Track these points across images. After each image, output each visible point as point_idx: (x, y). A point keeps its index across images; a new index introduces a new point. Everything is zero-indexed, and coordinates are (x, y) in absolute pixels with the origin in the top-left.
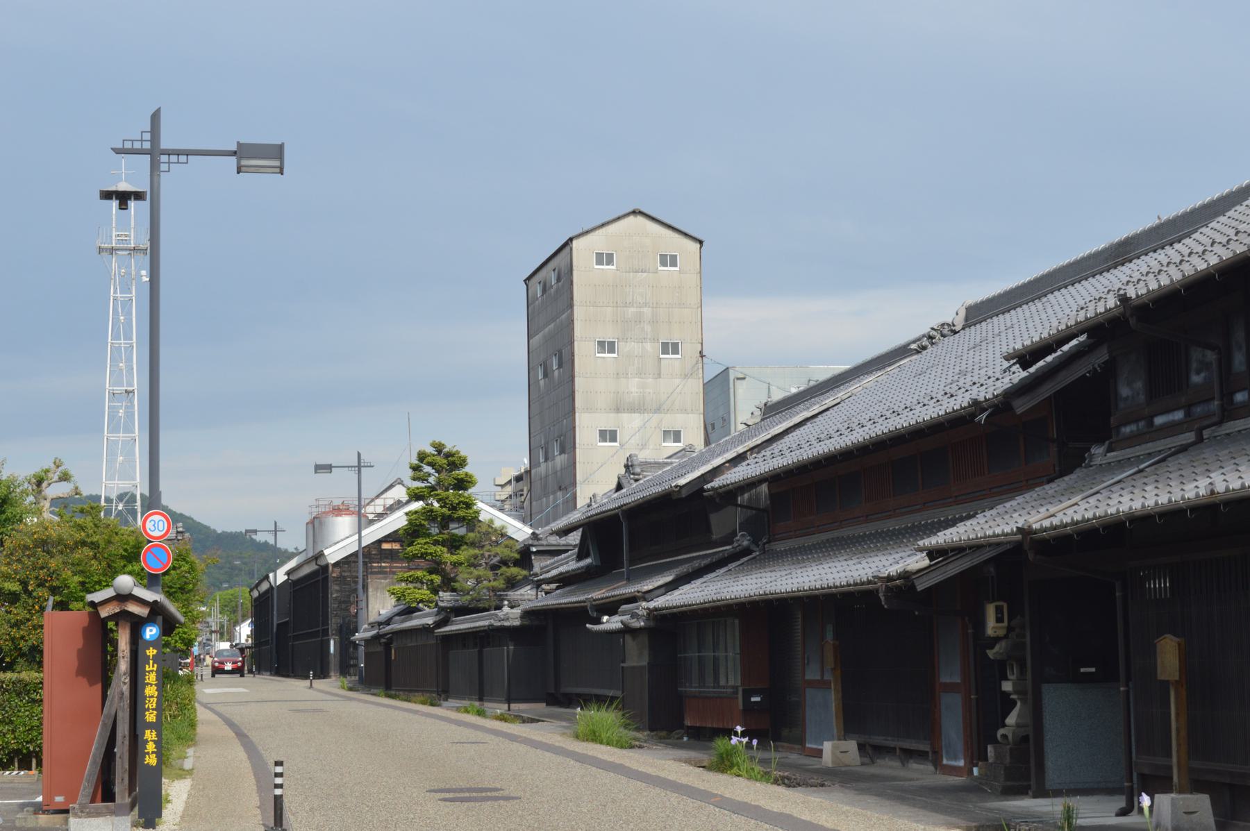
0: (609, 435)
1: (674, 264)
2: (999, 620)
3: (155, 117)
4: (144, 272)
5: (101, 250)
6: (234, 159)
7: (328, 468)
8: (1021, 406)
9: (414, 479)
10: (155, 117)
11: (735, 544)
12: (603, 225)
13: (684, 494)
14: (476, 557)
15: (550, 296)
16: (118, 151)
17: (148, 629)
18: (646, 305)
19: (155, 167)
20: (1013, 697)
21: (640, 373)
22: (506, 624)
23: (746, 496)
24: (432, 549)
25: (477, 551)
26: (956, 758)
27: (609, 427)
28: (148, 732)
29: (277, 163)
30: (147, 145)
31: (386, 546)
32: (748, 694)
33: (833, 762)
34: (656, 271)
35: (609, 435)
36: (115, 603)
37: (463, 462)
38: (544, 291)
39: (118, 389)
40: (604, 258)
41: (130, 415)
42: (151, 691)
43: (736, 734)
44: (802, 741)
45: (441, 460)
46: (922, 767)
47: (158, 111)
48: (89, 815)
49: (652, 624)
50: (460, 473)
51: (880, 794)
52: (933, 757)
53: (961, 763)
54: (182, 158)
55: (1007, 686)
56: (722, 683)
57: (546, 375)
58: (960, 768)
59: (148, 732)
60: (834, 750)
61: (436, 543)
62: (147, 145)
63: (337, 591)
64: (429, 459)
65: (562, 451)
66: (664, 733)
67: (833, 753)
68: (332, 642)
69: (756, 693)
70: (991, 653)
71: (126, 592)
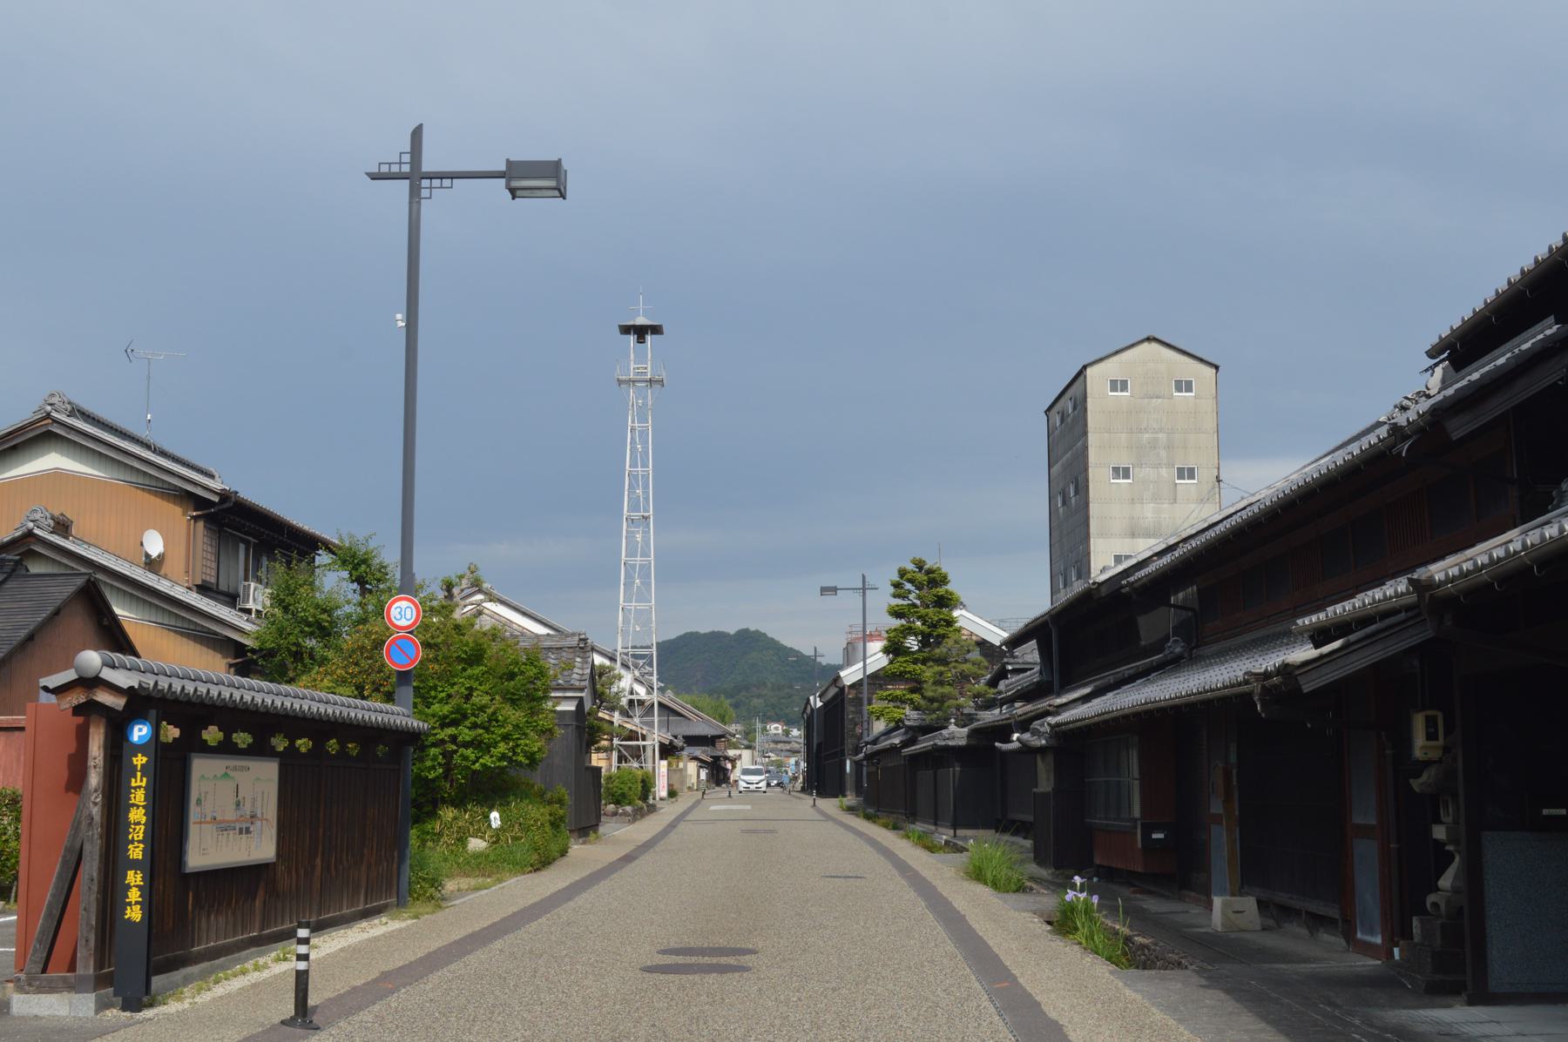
1: (1189, 389)
2: (1431, 736)
3: (417, 134)
4: (399, 316)
5: (620, 382)
6: (503, 181)
7: (834, 590)
8: (1458, 428)
9: (895, 596)
10: (417, 134)
12: (1117, 352)
13: (1104, 591)
14: (941, 674)
15: (1068, 421)
16: (374, 177)
17: (136, 728)
18: (1161, 430)
19: (415, 193)
20: (1450, 848)
21: (1156, 498)
22: (950, 743)
23: (1181, 595)
24: (911, 667)
26: (1372, 933)
28: (131, 873)
29: (552, 183)
30: (406, 168)
36: (78, 690)
37: (944, 580)
38: (1062, 420)
40: (1119, 385)
42: (137, 815)
43: (1073, 887)
45: (921, 577)
47: (420, 127)
48: (39, 990)
50: (941, 591)
51: (1236, 991)
52: (1346, 927)
53: (1378, 940)
54: (447, 182)
55: (1439, 833)
57: (1064, 503)
58: (1376, 945)
59: (131, 873)
60: (1225, 910)
61: (915, 662)
62: (406, 168)
64: (909, 576)
65: (1079, 577)
67: (1223, 913)
70: (1416, 784)
71: (91, 674)
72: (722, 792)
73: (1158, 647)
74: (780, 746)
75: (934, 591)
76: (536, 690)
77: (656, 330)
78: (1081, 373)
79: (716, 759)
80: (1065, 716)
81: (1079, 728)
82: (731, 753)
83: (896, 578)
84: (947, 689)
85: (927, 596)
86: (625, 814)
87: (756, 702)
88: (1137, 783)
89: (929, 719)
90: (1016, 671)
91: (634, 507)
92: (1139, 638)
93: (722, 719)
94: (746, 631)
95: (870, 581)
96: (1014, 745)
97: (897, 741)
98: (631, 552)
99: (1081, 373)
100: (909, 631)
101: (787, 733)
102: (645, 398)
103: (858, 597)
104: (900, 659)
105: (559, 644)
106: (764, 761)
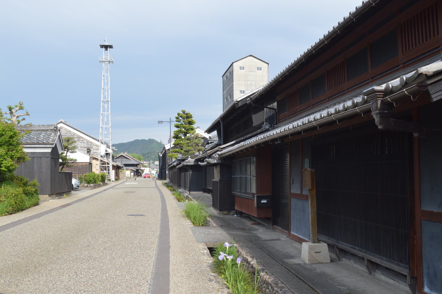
7: (162, 122)
11: (263, 128)
12: (242, 59)
13: (240, 105)
14: (188, 143)
18: (253, 81)
22: (189, 164)
25: (188, 141)
32: (259, 198)
33: (309, 260)
34: (256, 72)
37: (191, 117)
39: (105, 100)
40: (242, 68)
41: (108, 108)
45: (184, 116)
46: (391, 281)
49: (220, 161)
50: (190, 120)
56: (248, 191)
57: (227, 101)
64: (180, 115)
66: (226, 212)
67: (310, 253)
69: (264, 198)
72: (138, 179)
73: (260, 126)
75: (188, 120)
76: (13, 141)
77: (111, 47)
78: (232, 65)
79: (137, 170)
80: (224, 151)
81: (230, 155)
82: (142, 168)
83: (177, 116)
84: (190, 148)
85: (186, 122)
86: (90, 187)
87: (153, 156)
88: (254, 178)
89: (184, 157)
90: (211, 143)
91: (105, 97)
92: (252, 123)
93: (140, 160)
94: (150, 139)
96: (205, 163)
97: (175, 164)
98: (104, 111)
99: (232, 65)
100: (180, 131)
102: (108, 66)
103: (169, 124)
104: (178, 140)
105: (47, 129)
106: (151, 170)
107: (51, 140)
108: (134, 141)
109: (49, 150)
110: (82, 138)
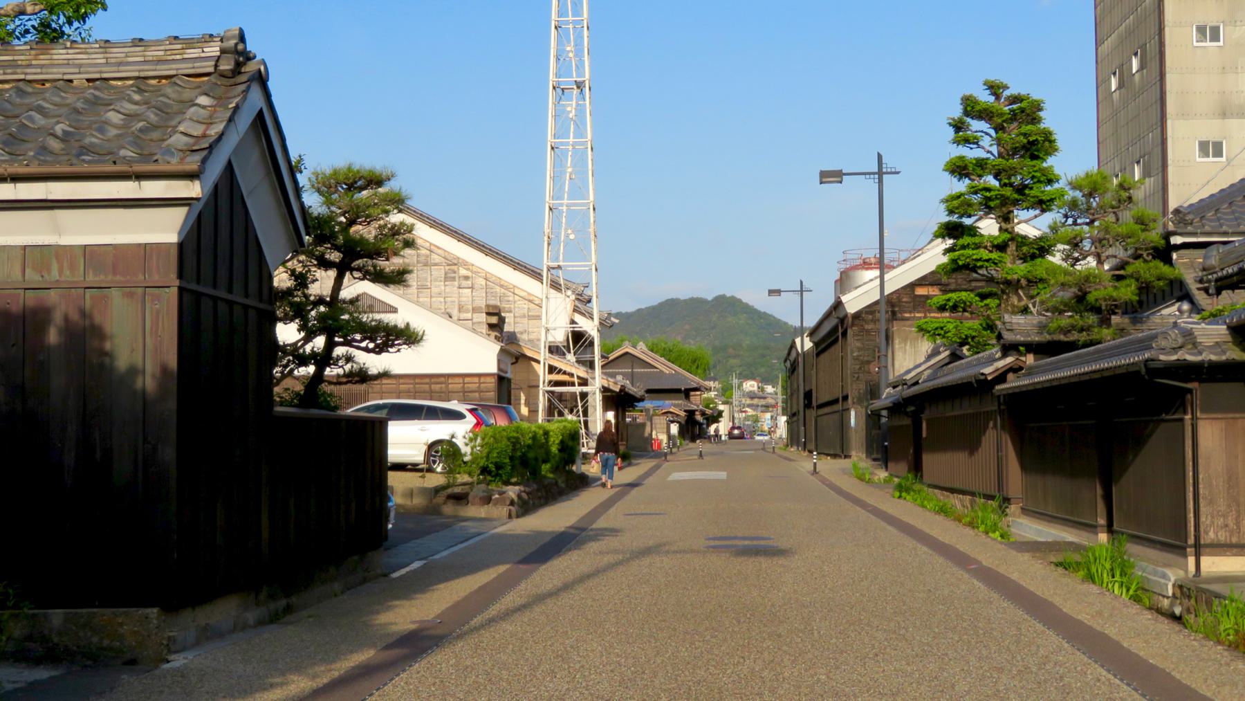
0: (1212, 148)
9: (957, 142)
27: (1212, 137)
31: (921, 291)
35: (1212, 148)
44: (1176, 536)
63: (859, 349)
68: (853, 413)
74: (756, 401)
87: (733, 361)
94: (723, 297)
95: (889, 162)
101: (762, 389)
103: (871, 185)
107: (178, 140)
108: (662, 305)
109: (164, 229)
110: (465, 264)
